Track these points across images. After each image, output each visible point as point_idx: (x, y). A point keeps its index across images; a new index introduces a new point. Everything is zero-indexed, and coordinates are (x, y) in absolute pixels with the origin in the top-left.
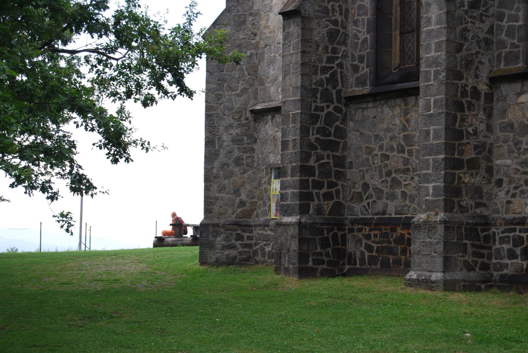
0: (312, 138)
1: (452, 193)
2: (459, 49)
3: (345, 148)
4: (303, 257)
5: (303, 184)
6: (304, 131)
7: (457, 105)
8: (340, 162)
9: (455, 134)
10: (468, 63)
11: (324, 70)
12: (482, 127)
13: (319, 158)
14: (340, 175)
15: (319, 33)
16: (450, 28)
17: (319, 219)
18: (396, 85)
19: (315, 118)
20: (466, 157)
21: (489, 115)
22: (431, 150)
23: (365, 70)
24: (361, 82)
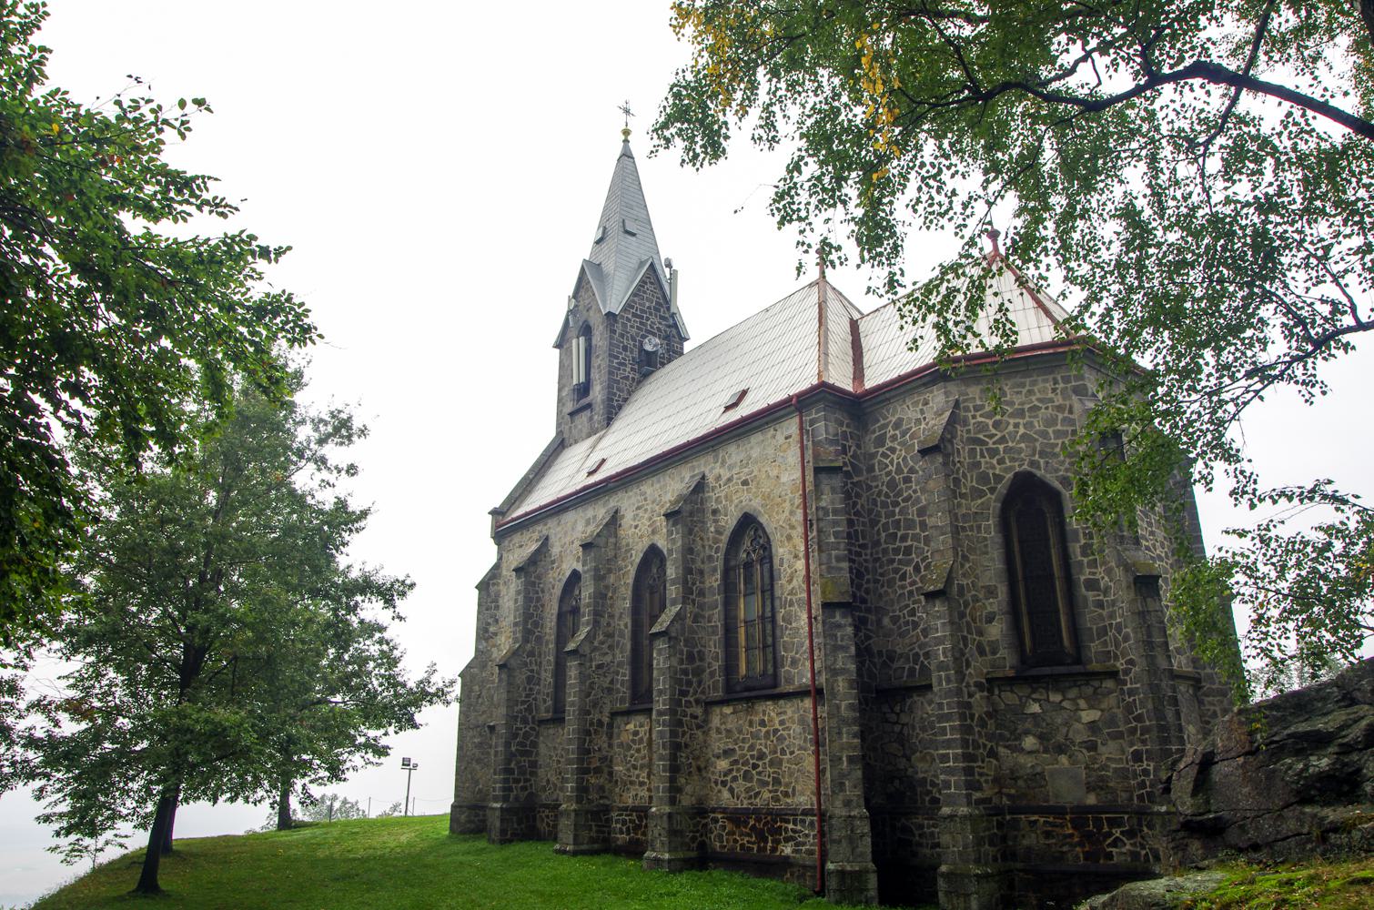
0: (513, 749)
1: (582, 790)
2: (588, 695)
3: (537, 754)
4: (503, 832)
5: (506, 781)
6: (507, 745)
7: (585, 734)
8: (534, 764)
9: (584, 752)
10: (595, 704)
11: (523, 703)
12: (606, 745)
13: (518, 762)
14: (534, 774)
15: (521, 677)
16: (582, 682)
17: (517, 805)
18: (640, 701)
19: (515, 736)
20: (592, 766)
21: (610, 736)
22: (569, 762)
23: (550, 703)
24: (547, 711)
